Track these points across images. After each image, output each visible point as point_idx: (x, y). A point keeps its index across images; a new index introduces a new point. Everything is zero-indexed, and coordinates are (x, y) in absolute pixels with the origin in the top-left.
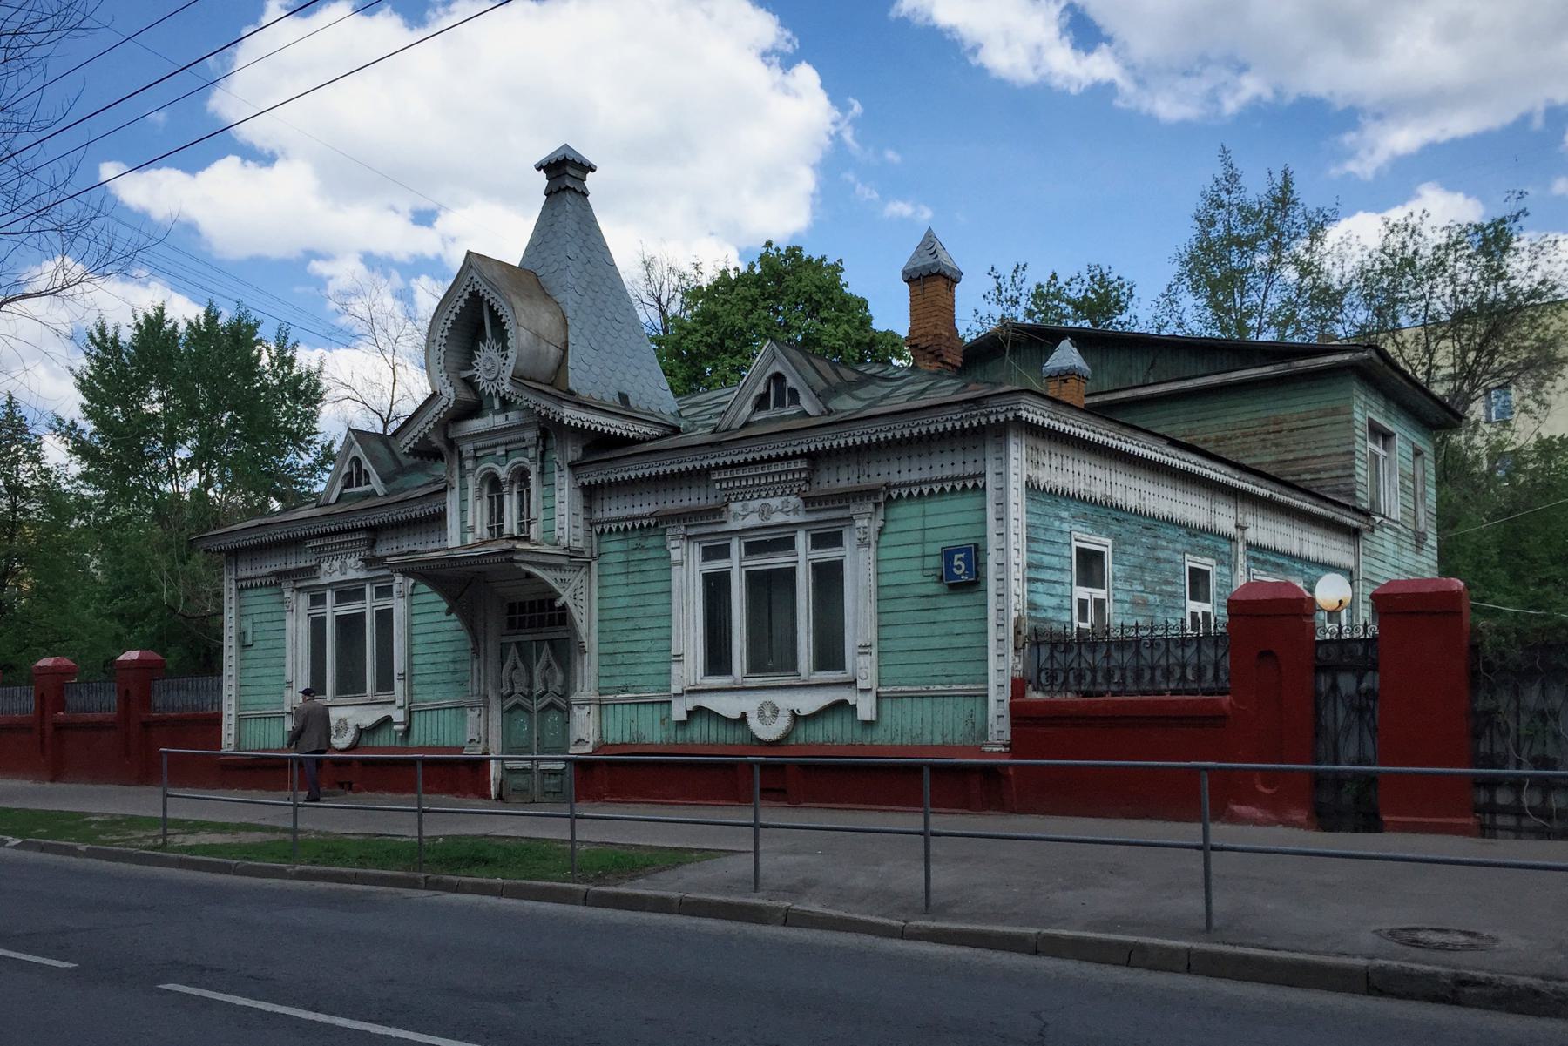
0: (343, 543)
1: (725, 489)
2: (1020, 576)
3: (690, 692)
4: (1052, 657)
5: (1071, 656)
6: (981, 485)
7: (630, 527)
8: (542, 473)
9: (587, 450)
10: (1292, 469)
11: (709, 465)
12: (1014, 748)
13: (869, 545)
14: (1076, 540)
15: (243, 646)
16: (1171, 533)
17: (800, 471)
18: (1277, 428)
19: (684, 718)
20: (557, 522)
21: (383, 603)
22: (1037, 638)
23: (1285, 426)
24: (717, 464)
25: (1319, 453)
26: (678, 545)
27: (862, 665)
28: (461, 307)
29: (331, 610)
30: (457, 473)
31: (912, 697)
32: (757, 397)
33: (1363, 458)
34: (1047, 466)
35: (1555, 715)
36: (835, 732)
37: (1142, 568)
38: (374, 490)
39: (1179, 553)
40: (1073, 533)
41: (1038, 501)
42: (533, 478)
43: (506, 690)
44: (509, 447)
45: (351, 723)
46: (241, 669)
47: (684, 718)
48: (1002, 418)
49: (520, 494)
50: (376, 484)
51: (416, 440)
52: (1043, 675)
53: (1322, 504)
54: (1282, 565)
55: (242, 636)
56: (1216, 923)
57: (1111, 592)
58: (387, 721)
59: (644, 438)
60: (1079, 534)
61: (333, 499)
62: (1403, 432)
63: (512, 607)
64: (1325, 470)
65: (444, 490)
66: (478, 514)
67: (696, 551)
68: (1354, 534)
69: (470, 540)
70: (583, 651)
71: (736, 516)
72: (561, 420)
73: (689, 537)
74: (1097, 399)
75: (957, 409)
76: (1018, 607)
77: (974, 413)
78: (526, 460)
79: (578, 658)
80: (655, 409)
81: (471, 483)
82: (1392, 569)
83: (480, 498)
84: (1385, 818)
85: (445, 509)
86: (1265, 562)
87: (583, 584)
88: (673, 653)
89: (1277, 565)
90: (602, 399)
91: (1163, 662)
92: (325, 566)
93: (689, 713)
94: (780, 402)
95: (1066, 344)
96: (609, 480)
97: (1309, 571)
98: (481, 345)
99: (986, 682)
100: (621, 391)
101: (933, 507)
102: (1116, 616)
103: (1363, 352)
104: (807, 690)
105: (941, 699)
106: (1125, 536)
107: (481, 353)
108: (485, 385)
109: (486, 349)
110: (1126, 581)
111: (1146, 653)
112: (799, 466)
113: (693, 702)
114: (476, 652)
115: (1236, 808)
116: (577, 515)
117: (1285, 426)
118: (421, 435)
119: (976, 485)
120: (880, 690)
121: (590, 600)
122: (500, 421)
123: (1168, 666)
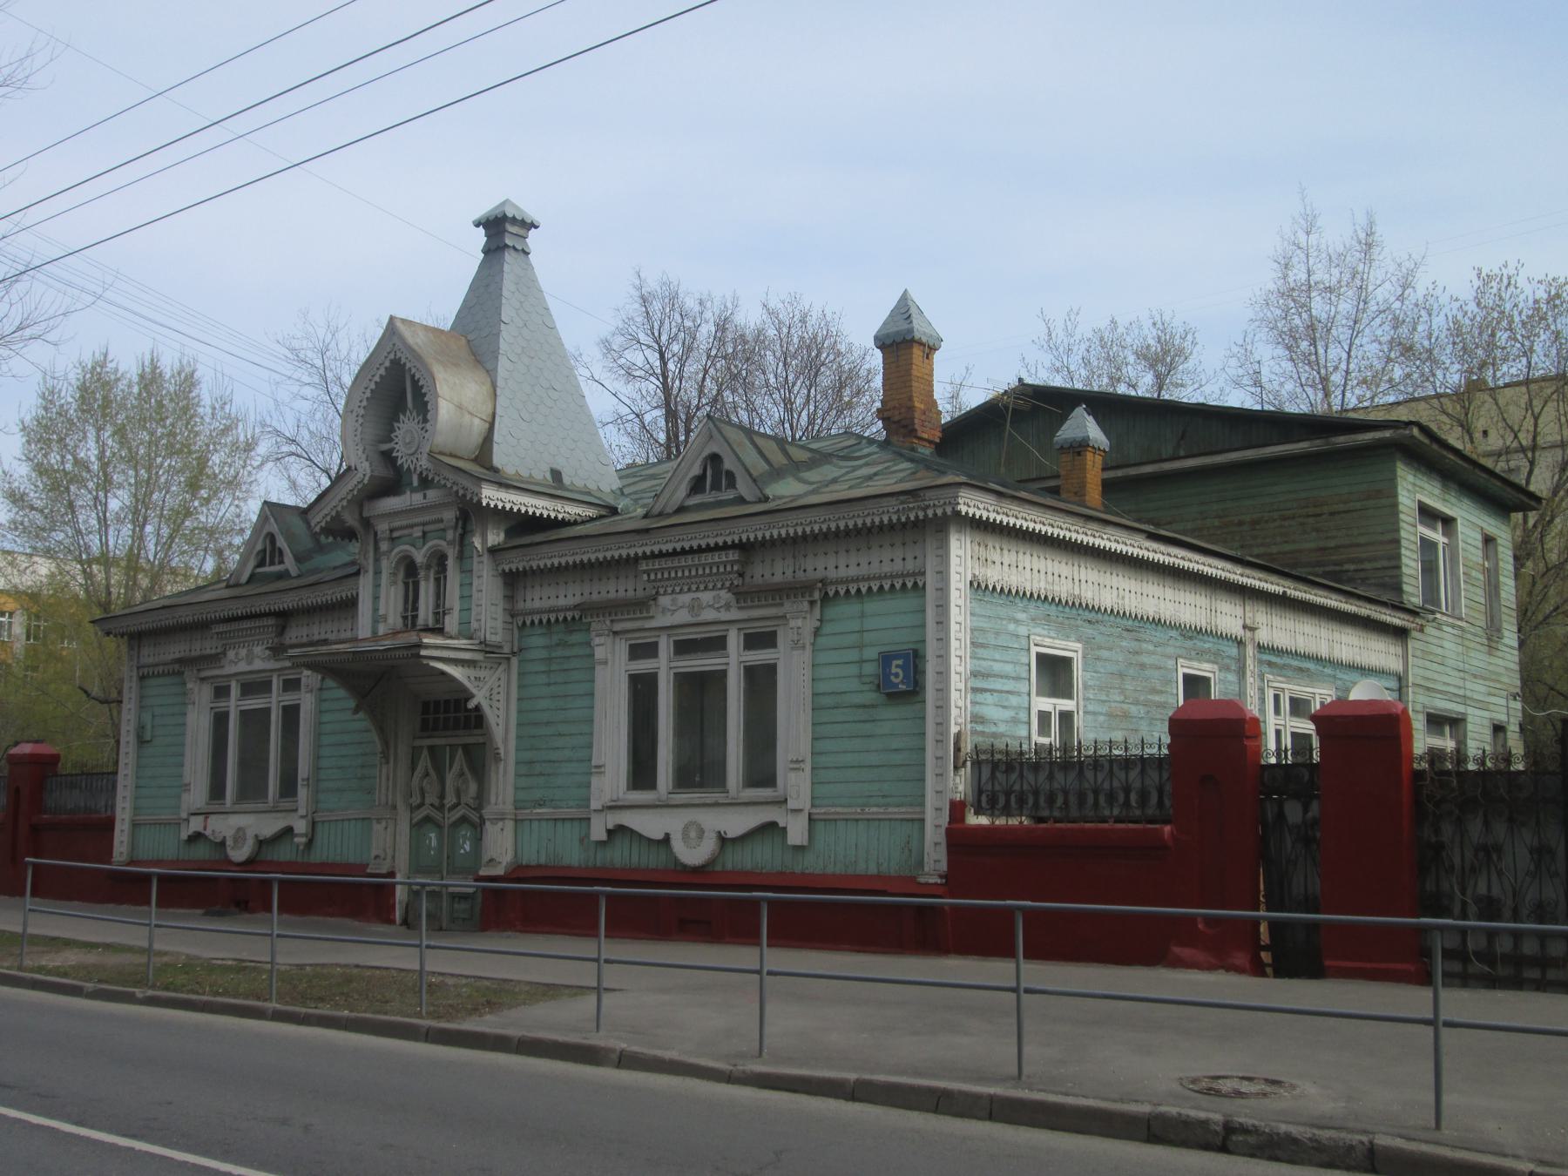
0: (251, 629)
1: (654, 581)
2: (962, 686)
3: (610, 808)
4: (993, 777)
5: (1014, 776)
6: (920, 584)
7: (553, 620)
8: (461, 557)
9: (510, 533)
10: (1334, 558)
11: (636, 554)
12: (954, 881)
13: (803, 647)
14: (1036, 645)
15: (142, 742)
16: (1159, 635)
17: (733, 563)
18: (1318, 510)
19: (604, 837)
20: (474, 613)
21: (289, 698)
22: (978, 756)
23: (1326, 509)
24: (644, 553)
25: (1362, 540)
26: (602, 642)
27: (796, 784)
28: (381, 376)
29: (235, 704)
30: (371, 554)
31: (847, 820)
32: (692, 479)
33: (1413, 547)
34: (998, 563)
35: (1498, 849)
36: (761, 858)
37: (1121, 675)
38: (287, 570)
39: (1169, 657)
40: (1032, 637)
41: (987, 602)
42: (450, 563)
43: (416, 800)
44: (427, 528)
45: (250, 834)
46: (139, 766)
47: (604, 837)
48: (939, 512)
49: (437, 580)
50: (289, 563)
51: (328, 519)
52: (984, 798)
53: (1351, 601)
54: (1308, 670)
55: (141, 729)
56: (1026, 1070)
57: (1081, 703)
58: (288, 831)
59: (575, 521)
60: (1038, 638)
61: (244, 579)
62: (1467, 516)
63: (426, 705)
64: (1369, 560)
65: (357, 573)
66: (392, 601)
67: (622, 648)
68: (1400, 634)
69: (382, 630)
70: (497, 758)
71: (664, 611)
72: (480, 502)
73: (615, 633)
74: (1120, 473)
75: (893, 501)
76: (960, 721)
77: (911, 505)
78: (444, 543)
79: (493, 768)
80: (592, 486)
81: (386, 565)
82: (1456, 673)
83: (395, 583)
84: (1327, 963)
85: (357, 595)
86: (1284, 667)
87: (502, 683)
89: (1301, 670)
91: (1106, 786)
92: (231, 654)
93: (609, 832)
94: (716, 486)
95: (1080, 411)
96: (531, 567)
97: (1345, 677)
98: (401, 417)
99: (923, 804)
100: (555, 466)
101: (872, 606)
102: (1088, 732)
103: (1405, 429)
104: (669, 810)
105: (877, 822)
106: (1099, 639)
107: (401, 425)
108: (404, 459)
109: (406, 421)
110: (1101, 689)
111: (1089, 774)
112: (731, 558)
113: (614, 819)
114: (385, 757)
115: (1177, 950)
117: (1326, 509)
118: (334, 513)
119: (915, 584)
120: (814, 811)
121: (508, 700)
122: (417, 499)
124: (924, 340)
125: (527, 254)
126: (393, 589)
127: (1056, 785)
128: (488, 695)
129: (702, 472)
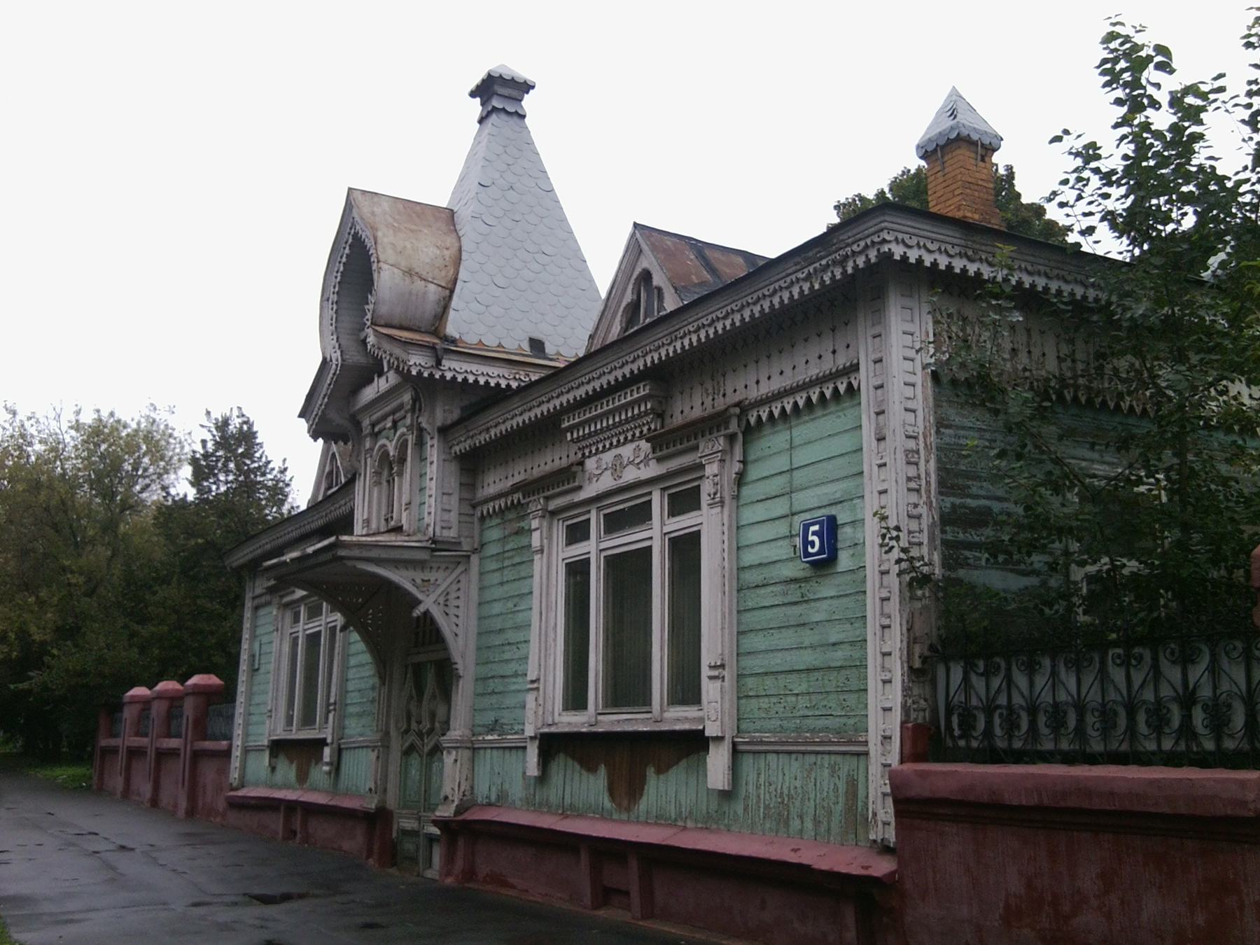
6: (855, 385)
15: (254, 671)
48: (861, 262)
73: (553, 513)
77: (824, 262)
83: (378, 483)
88: (529, 678)
90: (500, 345)
91: (1149, 695)
100: (537, 335)
101: (804, 430)
116: (450, 494)
123: (1159, 701)
124: (975, 137)
125: (523, 117)
126: (376, 489)
127: (1062, 697)
128: (441, 600)
129: (635, 297)
